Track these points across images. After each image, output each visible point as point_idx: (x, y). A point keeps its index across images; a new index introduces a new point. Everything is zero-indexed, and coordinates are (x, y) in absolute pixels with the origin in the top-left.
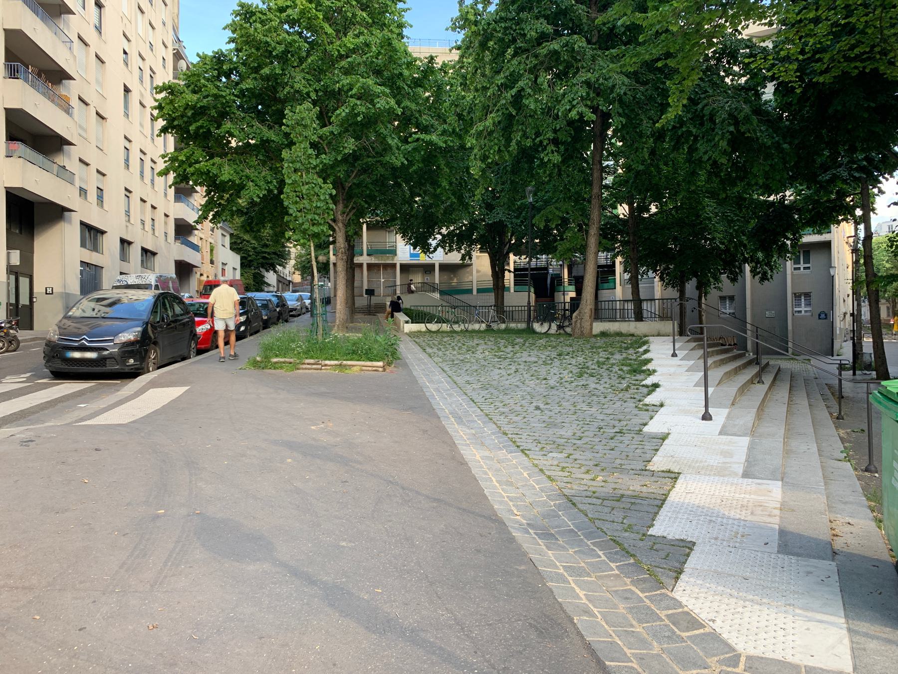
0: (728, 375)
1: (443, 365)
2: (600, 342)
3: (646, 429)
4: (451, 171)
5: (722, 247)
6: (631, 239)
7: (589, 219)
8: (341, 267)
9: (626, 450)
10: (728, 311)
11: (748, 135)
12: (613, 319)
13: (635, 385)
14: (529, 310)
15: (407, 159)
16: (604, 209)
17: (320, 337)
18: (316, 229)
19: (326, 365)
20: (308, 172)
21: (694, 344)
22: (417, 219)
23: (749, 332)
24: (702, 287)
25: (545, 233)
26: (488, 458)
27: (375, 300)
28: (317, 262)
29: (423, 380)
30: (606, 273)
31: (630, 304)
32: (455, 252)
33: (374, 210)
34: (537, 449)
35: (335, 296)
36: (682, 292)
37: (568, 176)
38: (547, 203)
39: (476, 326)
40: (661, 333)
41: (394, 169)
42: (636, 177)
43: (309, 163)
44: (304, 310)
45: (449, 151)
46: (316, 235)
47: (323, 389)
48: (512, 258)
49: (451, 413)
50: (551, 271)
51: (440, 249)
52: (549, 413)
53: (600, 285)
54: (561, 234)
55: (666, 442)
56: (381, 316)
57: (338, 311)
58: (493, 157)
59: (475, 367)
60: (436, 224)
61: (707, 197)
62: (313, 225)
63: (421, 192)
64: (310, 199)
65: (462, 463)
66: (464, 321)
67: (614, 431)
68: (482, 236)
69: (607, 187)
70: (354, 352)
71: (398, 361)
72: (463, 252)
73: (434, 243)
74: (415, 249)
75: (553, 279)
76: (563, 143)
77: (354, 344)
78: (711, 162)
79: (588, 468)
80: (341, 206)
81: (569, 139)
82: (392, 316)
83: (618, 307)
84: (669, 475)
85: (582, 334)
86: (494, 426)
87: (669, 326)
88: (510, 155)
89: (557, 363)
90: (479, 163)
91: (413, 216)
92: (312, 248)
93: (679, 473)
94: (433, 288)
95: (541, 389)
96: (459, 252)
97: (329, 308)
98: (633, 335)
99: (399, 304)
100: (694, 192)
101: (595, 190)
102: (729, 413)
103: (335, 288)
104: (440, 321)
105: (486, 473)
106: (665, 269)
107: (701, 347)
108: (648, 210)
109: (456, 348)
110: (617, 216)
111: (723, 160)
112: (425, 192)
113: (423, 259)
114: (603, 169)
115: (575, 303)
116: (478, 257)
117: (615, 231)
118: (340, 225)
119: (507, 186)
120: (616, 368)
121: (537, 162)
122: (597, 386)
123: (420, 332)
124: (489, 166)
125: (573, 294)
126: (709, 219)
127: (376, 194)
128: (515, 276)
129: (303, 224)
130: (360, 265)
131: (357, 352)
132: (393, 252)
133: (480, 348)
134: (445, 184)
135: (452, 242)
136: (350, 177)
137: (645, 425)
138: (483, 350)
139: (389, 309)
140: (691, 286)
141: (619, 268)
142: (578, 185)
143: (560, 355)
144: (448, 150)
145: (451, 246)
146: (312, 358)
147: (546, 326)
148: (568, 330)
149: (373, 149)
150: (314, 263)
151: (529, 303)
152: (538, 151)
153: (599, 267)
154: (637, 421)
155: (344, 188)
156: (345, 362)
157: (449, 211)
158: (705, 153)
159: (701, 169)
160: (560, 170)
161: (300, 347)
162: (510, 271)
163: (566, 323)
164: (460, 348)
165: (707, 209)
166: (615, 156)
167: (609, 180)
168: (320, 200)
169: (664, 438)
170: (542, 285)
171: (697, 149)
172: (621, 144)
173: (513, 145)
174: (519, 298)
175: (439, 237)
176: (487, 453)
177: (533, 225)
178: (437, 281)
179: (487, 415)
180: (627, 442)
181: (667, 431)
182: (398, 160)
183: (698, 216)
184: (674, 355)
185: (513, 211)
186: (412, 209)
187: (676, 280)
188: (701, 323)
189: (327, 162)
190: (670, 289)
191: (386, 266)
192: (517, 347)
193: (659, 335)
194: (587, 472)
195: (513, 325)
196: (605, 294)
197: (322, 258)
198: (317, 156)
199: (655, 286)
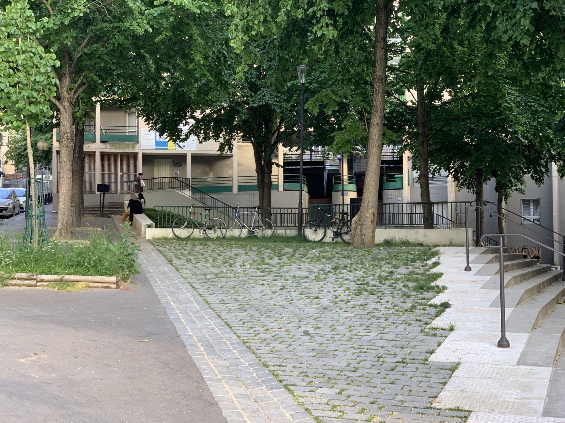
0: (530, 292)
1: (193, 281)
2: (383, 252)
3: (432, 358)
4: (207, 43)
5: (525, 142)
6: (420, 132)
7: (371, 106)
8: (66, 156)
9: (409, 383)
10: (532, 217)
11: (553, 13)
12: (399, 225)
13: (421, 304)
14: (301, 214)
15: (152, 27)
16: (390, 94)
17: (35, 246)
18: (33, 109)
19: (42, 281)
20: (25, 38)
21: (493, 256)
22: (164, 99)
23: (556, 244)
24: (502, 189)
25: (322, 118)
26: (243, 396)
27: (109, 198)
28: (35, 150)
29: (167, 300)
30: (391, 170)
31: (418, 207)
32: (212, 141)
33: (111, 87)
34: (304, 384)
35: (58, 192)
36: (479, 194)
37: (348, 54)
38: (323, 84)
39: (236, 233)
40: (454, 242)
41: (136, 37)
42: (426, 57)
43: (27, 27)
44: (17, 210)
45: (205, 19)
46: (33, 117)
47: (37, 311)
48: (281, 149)
49: (200, 341)
50: (328, 166)
51: (193, 137)
52: (320, 340)
53: (386, 185)
54: (339, 123)
55: (456, 373)
56: (117, 218)
57: (60, 212)
58: (258, 29)
59: (232, 284)
60: (188, 106)
61: (508, 84)
62: (31, 103)
63: (170, 67)
64: (27, 72)
65: (211, 404)
66: (221, 226)
67: (396, 360)
68: (245, 122)
69: (392, 69)
70: (79, 264)
71: (136, 275)
72: (221, 140)
73: (185, 129)
74: (161, 135)
75: (330, 176)
76: (341, 15)
77: (80, 254)
78: (512, 43)
79: (363, 406)
80: (67, 81)
81: (346, 13)
82: (131, 219)
83: (405, 211)
84: (458, 413)
85: (363, 243)
86: (253, 356)
87: (460, 234)
88: (278, 27)
89: (331, 278)
90: (241, 35)
91: (159, 96)
92: (28, 133)
93: (470, 412)
94: (184, 184)
95: (312, 310)
96: (216, 140)
97: (49, 208)
98: (421, 245)
99: (140, 204)
100: (492, 77)
101: (379, 73)
102: (529, 339)
103: (58, 182)
104: (192, 225)
105: (240, 415)
106: (459, 167)
107: (498, 259)
108: (440, 98)
109: (210, 259)
110: (403, 104)
111: (525, 41)
112: (174, 67)
113: (172, 148)
114: (388, 48)
115: (356, 204)
116: (239, 147)
117: (402, 121)
118: (66, 104)
119: (275, 63)
120: (400, 285)
121: (311, 37)
122: (378, 306)
123: (166, 238)
124: (253, 39)
125: (354, 195)
126: (510, 109)
127: (113, 67)
128: (285, 171)
129: (17, 102)
130: (92, 155)
131: (83, 264)
132: (135, 139)
133: (239, 260)
134: (199, 58)
135: (207, 128)
136: (80, 45)
137: (432, 352)
138: (244, 261)
139: (127, 210)
140: (489, 187)
141: (407, 165)
142: (359, 66)
143: (335, 268)
144: (202, 18)
145: (206, 134)
146: (24, 271)
147: (320, 232)
148: (347, 238)
149: (110, 12)
150: (30, 151)
151: (300, 204)
152: (312, 24)
153: (383, 162)
154: (423, 348)
155: (71, 59)
156: (67, 277)
157: (204, 91)
158: (505, 32)
159: (501, 50)
160: (337, 47)
161: (9, 257)
162: (278, 165)
163: (345, 230)
164: (214, 260)
165: (507, 98)
166: (402, 32)
167: (395, 61)
168: (39, 73)
169: (453, 368)
170: (317, 182)
171: (495, 27)
172: (409, 18)
173: (282, 17)
174: (290, 198)
175: (192, 122)
176: (242, 390)
177: (306, 111)
178: (189, 175)
179: (244, 343)
180: (410, 374)
181: (457, 361)
182: (140, 27)
183: (498, 105)
184: (468, 269)
185: (283, 93)
186: (158, 87)
187: (472, 180)
188: (501, 231)
189: (51, 26)
190: (465, 190)
191: (125, 156)
192: (285, 259)
193: (451, 245)
194: (363, 411)
195: (281, 232)
196: (390, 195)
197: (42, 145)
198: (37, 19)
199: (448, 187)
